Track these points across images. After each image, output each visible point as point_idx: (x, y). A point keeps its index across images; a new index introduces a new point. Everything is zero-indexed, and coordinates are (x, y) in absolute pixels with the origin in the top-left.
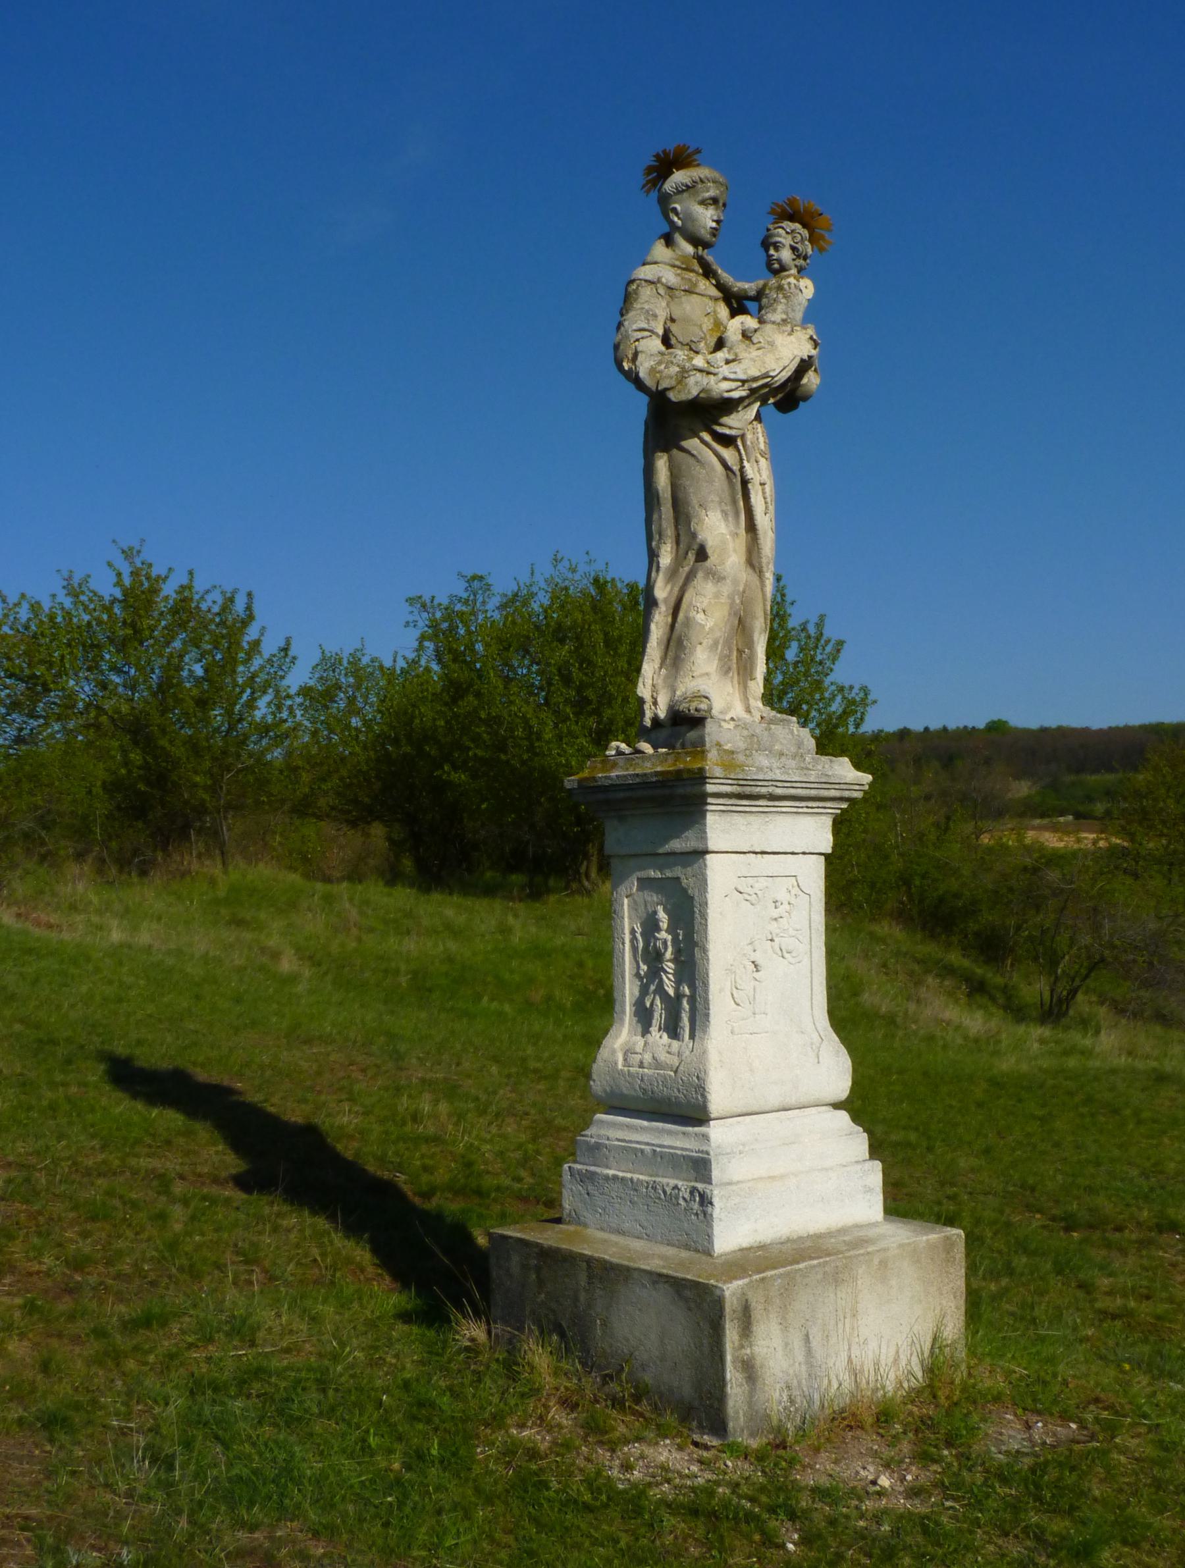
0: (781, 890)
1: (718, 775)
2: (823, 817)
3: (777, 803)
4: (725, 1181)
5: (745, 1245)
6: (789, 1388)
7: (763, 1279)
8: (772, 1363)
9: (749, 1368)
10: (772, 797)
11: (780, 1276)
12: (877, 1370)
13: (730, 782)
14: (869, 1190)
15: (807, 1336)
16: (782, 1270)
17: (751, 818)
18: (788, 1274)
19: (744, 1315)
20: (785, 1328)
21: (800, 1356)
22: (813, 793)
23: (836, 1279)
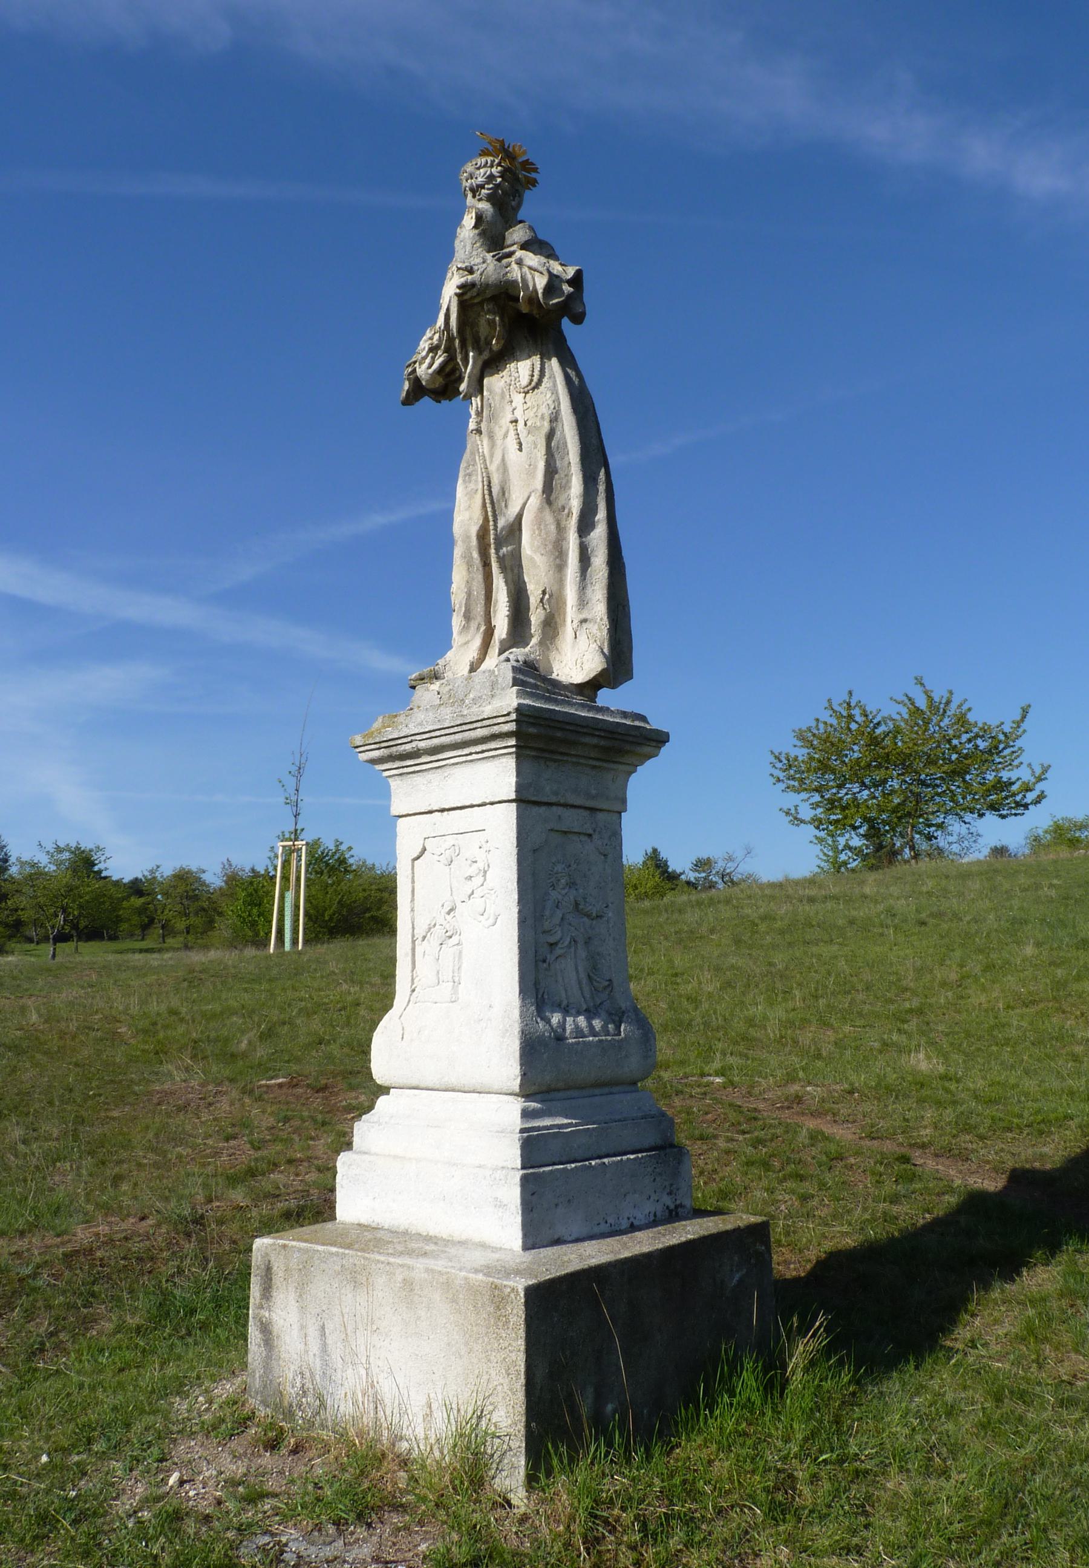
0: (471, 846)
1: (359, 744)
2: (504, 760)
3: (440, 756)
4: (363, 1149)
5: (363, 1221)
6: (301, 1373)
7: (284, 1246)
8: (287, 1338)
9: (266, 1329)
10: (415, 754)
11: (300, 1250)
12: (648, 1450)
13: (373, 747)
14: (500, 1205)
15: (323, 1327)
16: (303, 1245)
17: (429, 776)
18: (307, 1251)
19: (266, 1275)
20: (302, 1309)
21: (315, 1347)
22: (458, 737)
23: (356, 1278)
